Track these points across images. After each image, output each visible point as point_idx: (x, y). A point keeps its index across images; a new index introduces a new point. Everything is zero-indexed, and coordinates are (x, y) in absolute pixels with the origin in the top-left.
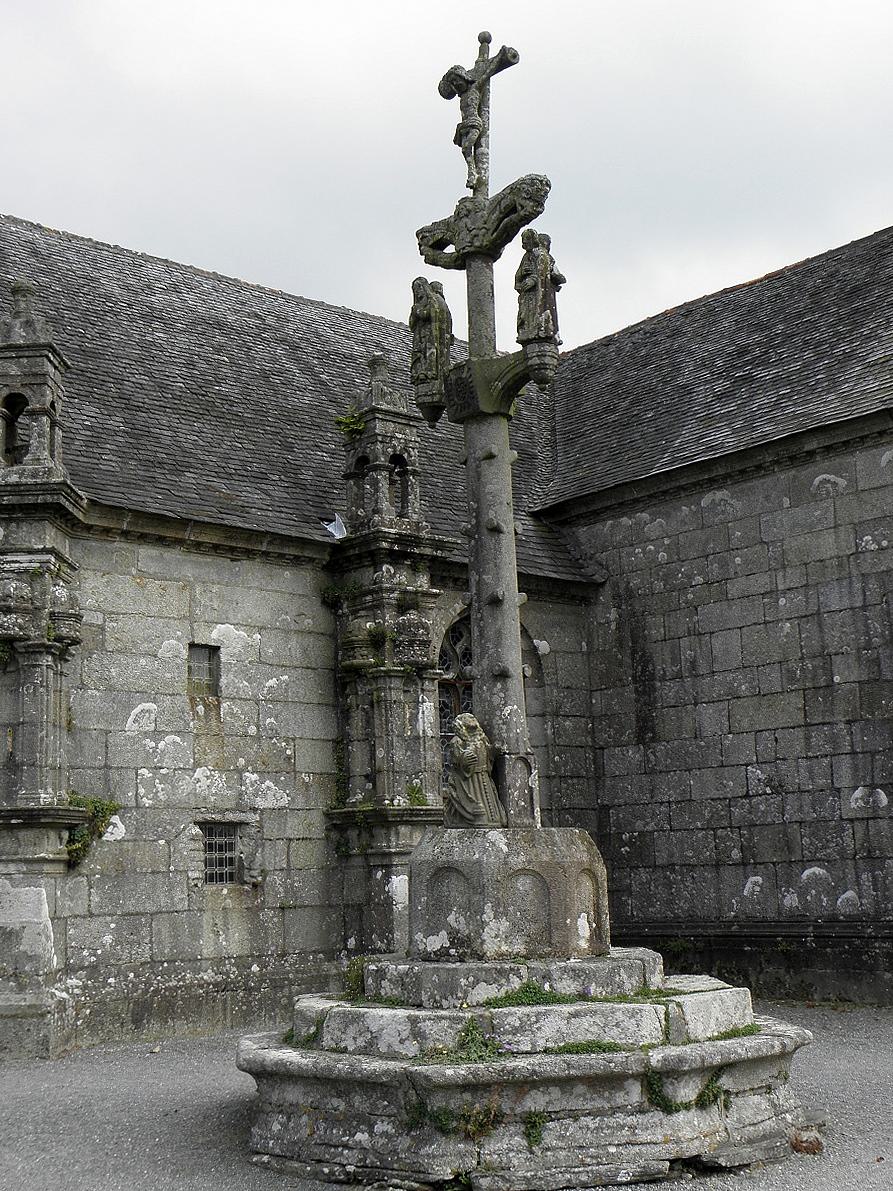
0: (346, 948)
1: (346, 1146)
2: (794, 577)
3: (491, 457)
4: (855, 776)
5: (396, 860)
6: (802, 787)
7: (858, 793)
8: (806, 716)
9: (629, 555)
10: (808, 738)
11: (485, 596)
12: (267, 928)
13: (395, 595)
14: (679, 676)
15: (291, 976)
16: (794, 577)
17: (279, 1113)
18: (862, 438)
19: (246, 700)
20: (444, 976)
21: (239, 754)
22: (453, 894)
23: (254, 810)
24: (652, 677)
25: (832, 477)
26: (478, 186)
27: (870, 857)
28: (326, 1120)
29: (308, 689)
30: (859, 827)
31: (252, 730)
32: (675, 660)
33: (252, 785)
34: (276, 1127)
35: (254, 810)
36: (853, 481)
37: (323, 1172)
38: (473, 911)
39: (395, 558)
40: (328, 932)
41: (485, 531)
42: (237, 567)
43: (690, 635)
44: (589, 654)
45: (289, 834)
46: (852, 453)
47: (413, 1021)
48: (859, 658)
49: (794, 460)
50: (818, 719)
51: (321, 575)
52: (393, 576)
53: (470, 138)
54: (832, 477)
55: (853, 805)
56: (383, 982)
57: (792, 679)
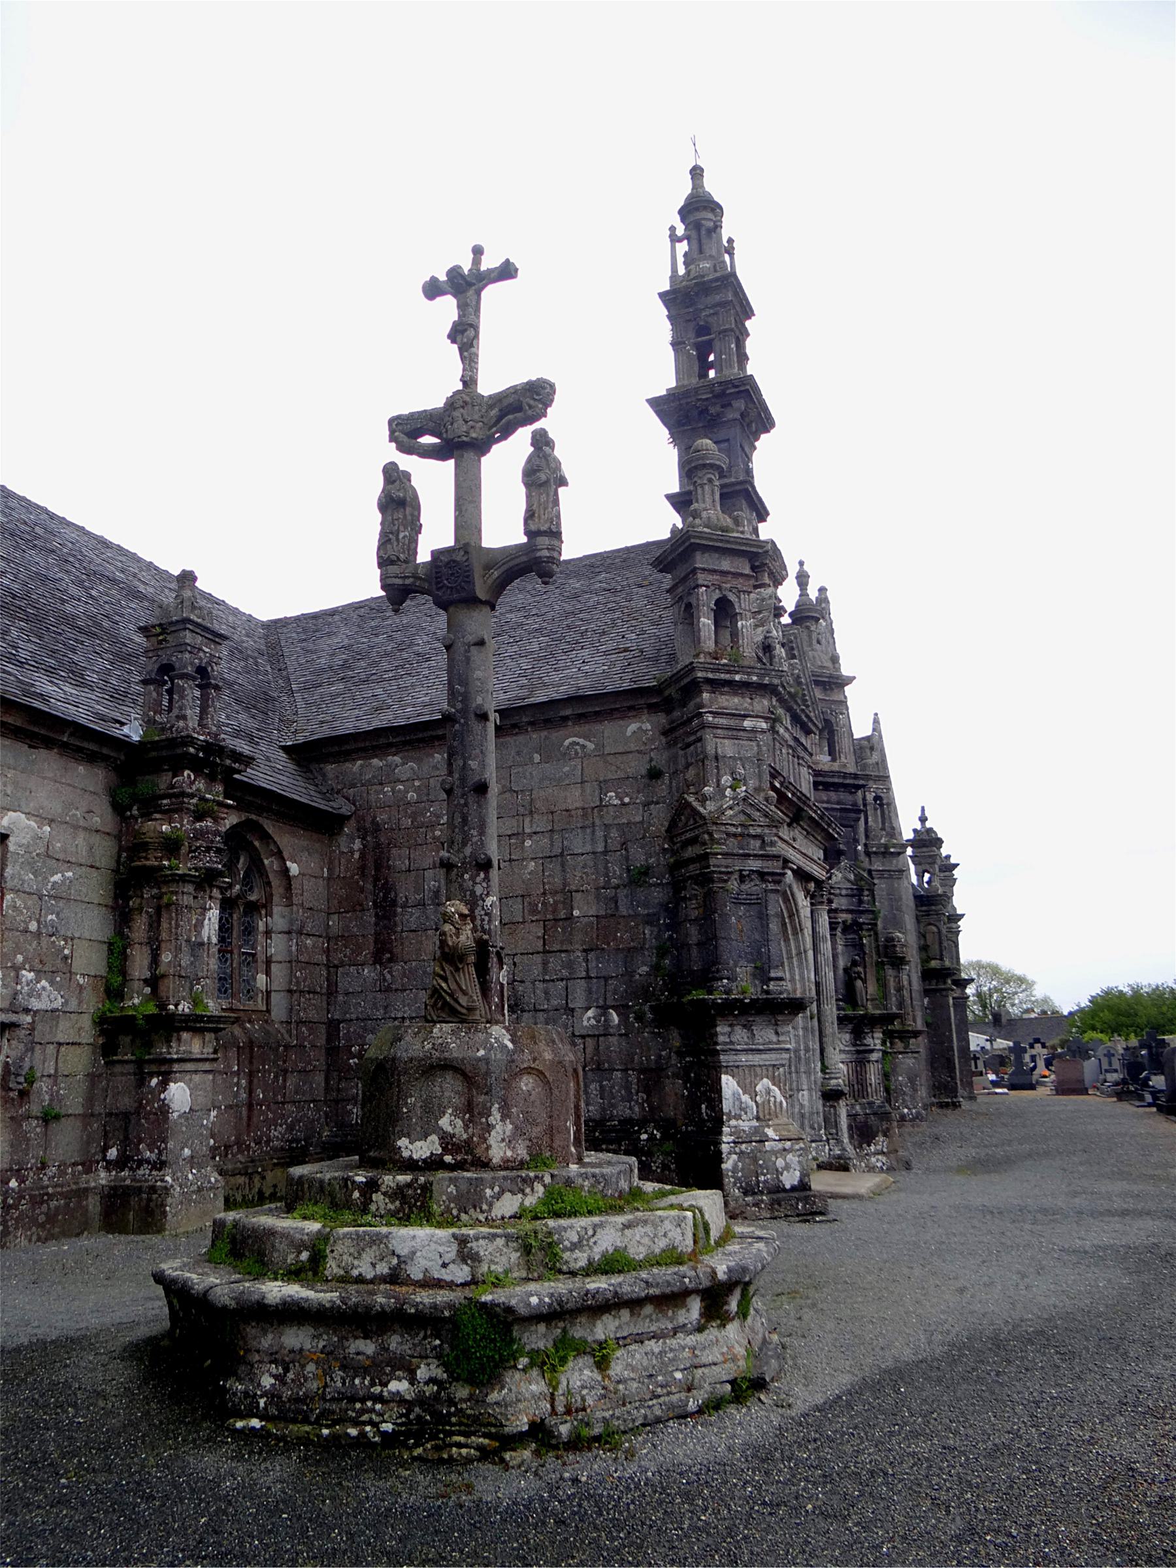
0: (104, 1159)
1: (379, 1398)
2: (541, 824)
3: (481, 643)
4: (588, 999)
5: (176, 1067)
6: (538, 1007)
7: (590, 1013)
8: (544, 944)
9: (378, 793)
10: (545, 964)
11: (470, 783)
12: (28, 1140)
13: (194, 801)
14: (422, 904)
15: (50, 1190)
16: (541, 824)
17: (271, 1362)
18: (612, 710)
19: (29, 893)
20: (464, 1187)
21: (18, 949)
22: (447, 1094)
23: (27, 1011)
24: (394, 903)
25: (581, 741)
26: (469, 381)
27: (599, 1069)
28: (343, 1367)
29: (94, 888)
30: (590, 1042)
31: (33, 926)
32: (419, 889)
33: (28, 985)
34: (267, 1381)
35: (27, 1011)
36: (600, 746)
37: (348, 1435)
38: (472, 1112)
39: (197, 766)
40: (88, 1143)
41: (472, 716)
42: (35, 754)
43: (435, 867)
44: (329, 879)
45: (61, 1038)
46: (601, 722)
47: (463, 1241)
48: (598, 897)
49: (548, 724)
50: (556, 947)
51: (112, 775)
52: (192, 783)
53: (464, 335)
54: (581, 741)
55: (585, 1023)
56: (374, 1196)
57: (534, 911)
